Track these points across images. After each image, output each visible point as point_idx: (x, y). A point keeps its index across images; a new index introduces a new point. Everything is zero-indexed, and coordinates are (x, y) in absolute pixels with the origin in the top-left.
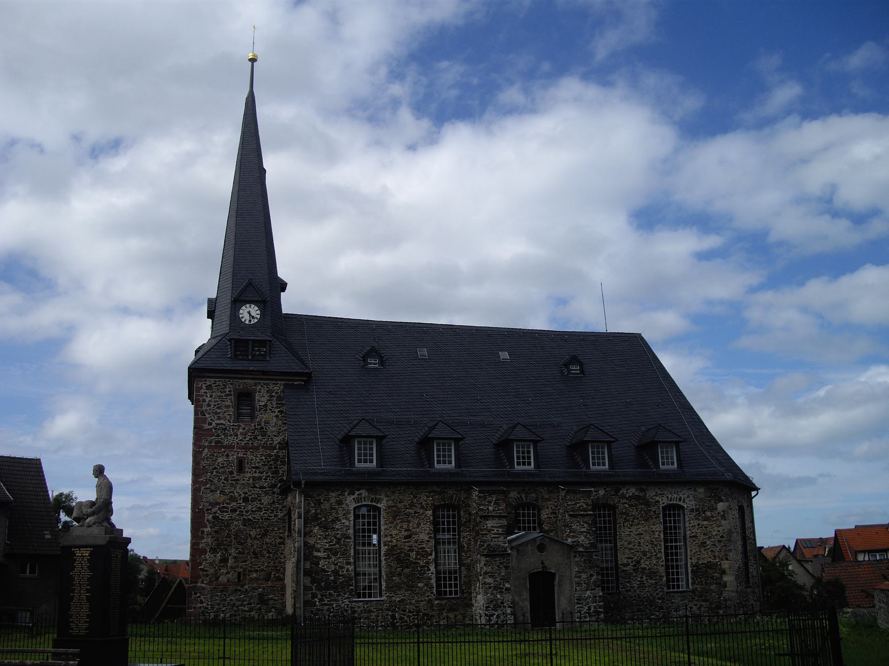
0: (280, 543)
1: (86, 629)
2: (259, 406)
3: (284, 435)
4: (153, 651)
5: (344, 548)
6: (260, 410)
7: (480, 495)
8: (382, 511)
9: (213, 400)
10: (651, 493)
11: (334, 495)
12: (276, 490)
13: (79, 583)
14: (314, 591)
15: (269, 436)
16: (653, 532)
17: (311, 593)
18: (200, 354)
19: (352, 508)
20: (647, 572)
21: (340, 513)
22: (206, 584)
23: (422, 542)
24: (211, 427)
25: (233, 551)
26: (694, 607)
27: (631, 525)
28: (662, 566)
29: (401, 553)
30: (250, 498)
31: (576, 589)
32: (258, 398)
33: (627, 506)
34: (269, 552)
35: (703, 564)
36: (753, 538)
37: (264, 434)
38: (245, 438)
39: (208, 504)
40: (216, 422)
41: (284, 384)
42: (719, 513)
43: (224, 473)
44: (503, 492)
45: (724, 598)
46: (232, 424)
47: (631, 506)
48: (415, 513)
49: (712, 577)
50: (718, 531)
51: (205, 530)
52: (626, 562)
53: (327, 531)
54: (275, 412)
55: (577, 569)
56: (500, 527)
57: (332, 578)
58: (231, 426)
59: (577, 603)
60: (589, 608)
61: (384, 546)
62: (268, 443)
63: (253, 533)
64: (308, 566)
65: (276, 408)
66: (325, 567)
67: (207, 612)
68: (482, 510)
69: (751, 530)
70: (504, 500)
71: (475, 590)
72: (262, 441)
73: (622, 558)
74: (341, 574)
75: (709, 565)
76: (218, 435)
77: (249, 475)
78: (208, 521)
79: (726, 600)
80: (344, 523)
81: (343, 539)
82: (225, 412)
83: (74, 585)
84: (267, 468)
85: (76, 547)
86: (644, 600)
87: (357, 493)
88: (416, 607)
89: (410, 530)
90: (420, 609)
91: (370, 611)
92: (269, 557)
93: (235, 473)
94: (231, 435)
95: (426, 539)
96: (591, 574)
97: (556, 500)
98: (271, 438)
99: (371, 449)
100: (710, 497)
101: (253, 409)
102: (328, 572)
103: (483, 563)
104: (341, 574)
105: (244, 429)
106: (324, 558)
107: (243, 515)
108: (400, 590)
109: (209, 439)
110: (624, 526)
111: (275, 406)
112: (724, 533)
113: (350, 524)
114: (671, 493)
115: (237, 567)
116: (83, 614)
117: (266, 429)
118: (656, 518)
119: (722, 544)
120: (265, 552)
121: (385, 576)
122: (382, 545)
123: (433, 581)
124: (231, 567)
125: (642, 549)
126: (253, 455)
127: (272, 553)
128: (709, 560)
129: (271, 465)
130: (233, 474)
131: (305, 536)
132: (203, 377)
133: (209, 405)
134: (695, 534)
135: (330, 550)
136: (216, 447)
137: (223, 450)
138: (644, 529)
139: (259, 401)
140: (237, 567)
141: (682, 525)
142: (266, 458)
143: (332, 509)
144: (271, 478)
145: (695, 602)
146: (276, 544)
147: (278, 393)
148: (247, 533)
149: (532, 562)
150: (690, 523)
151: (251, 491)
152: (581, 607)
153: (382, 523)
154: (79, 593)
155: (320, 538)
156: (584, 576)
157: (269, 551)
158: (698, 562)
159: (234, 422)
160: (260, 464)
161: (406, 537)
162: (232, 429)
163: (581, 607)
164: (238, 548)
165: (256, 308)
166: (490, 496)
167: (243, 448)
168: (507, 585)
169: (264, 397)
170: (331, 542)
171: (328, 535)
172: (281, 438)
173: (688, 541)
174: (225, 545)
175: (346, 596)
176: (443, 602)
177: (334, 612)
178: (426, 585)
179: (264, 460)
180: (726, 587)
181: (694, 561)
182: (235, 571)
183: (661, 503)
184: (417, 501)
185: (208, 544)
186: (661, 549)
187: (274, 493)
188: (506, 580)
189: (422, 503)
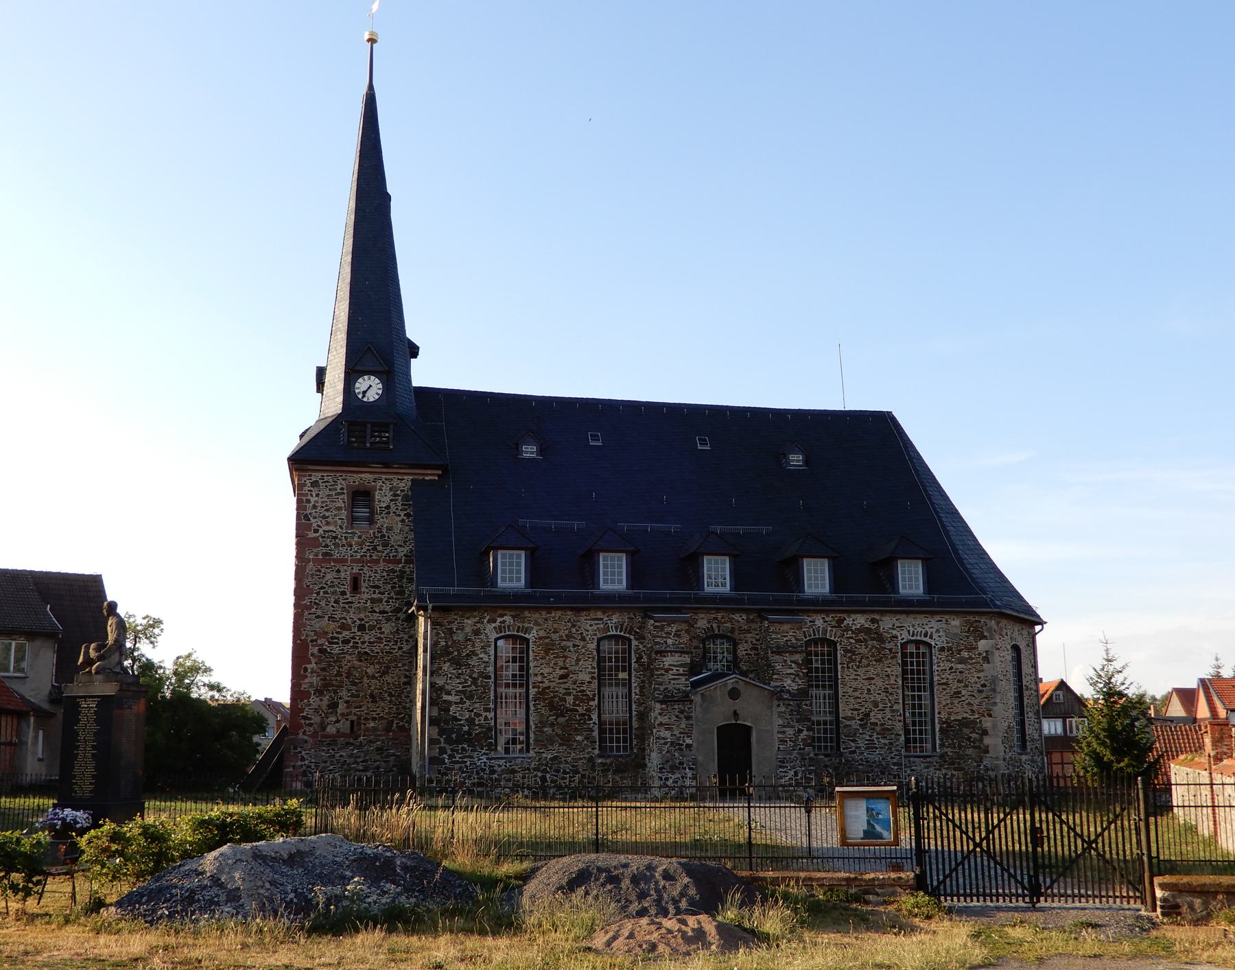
0: (405, 683)
1: (91, 792)
4: (1213, 806)
6: (381, 513)
7: (656, 624)
8: (531, 643)
9: (320, 500)
10: (887, 623)
11: (469, 622)
14: (442, 745)
15: (393, 546)
18: (306, 439)
19: (493, 640)
20: (878, 728)
22: (309, 736)
23: (582, 683)
24: (318, 534)
27: (858, 667)
28: (900, 721)
29: (555, 697)
30: (367, 625)
31: (779, 748)
33: (853, 641)
34: (390, 695)
35: (955, 720)
36: (1034, 688)
37: (385, 545)
38: (362, 549)
39: (313, 633)
40: (324, 528)
42: (980, 654)
43: (334, 593)
44: (685, 621)
45: (985, 766)
48: (574, 646)
50: (979, 678)
51: (309, 666)
54: (400, 515)
55: (781, 722)
56: (681, 666)
57: (466, 728)
59: (780, 767)
60: (796, 774)
61: (533, 688)
62: (391, 555)
64: (435, 713)
67: (310, 772)
68: (658, 643)
69: (1033, 678)
70: (687, 631)
71: (649, 745)
73: (844, 710)
74: (477, 723)
75: (964, 723)
76: (327, 546)
77: (365, 596)
78: (313, 655)
79: (987, 769)
81: (481, 679)
82: (335, 515)
83: (79, 741)
85: (81, 697)
86: (874, 765)
87: (499, 620)
88: (573, 766)
89: (567, 668)
90: (577, 770)
91: (513, 772)
92: (391, 702)
94: (343, 546)
95: (588, 680)
96: (799, 729)
98: (396, 549)
99: (519, 564)
100: (967, 632)
101: (372, 513)
102: (461, 720)
103: (657, 711)
104: (477, 723)
105: (360, 537)
106: (456, 703)
107: (357, 648)
108: (552, 745)
109: (315, 550)
111: (400, 508)
112: (986, 680)
113: (490, 659)
114: (913, 626)
115: (348, 714)
117: (388, 537)
118: (892, 658)
119: (984, 695)
120: (386, 695)
121: (533, 727)
122: (531, 687)
123: (596, 734)
124: (342, 715)
125: (873, 699)
128: (965, 715)
129: (396, 583)
131: (431, 675)
132: (307, 470)
133: (315, 507)
134: (945, 681)
136: (323, 561)
137: (332, 564)
138: (875, 673)
139: (380, 501)
140: (348, 714)
141: (927, 668)
143: (470, 640)
146: (399, 684)
147: (404, 491)
148: (362, 671)
149: (721, 713)
153: (531, 658)
156: (790, 731)
157: (390, 693)
158: (949, 718)
159: (347, 528)
161: (562, 677)
165: (377, 381)
166: (669, 625)
167: (358, 561)
168: (688, 741)
171: (462, 674)
173: (935, 689)
174: (333, 686)
175: (483, 751)
176: (608, 761)
178: (587, 738)
180: (988, 752)
181: (944, 716)
182: (347, 720)
183: (900, 638)
184: (576, 630)
185: (311, 685)
186: (898, 699)
188: (686, 733)
189: (582, 633)
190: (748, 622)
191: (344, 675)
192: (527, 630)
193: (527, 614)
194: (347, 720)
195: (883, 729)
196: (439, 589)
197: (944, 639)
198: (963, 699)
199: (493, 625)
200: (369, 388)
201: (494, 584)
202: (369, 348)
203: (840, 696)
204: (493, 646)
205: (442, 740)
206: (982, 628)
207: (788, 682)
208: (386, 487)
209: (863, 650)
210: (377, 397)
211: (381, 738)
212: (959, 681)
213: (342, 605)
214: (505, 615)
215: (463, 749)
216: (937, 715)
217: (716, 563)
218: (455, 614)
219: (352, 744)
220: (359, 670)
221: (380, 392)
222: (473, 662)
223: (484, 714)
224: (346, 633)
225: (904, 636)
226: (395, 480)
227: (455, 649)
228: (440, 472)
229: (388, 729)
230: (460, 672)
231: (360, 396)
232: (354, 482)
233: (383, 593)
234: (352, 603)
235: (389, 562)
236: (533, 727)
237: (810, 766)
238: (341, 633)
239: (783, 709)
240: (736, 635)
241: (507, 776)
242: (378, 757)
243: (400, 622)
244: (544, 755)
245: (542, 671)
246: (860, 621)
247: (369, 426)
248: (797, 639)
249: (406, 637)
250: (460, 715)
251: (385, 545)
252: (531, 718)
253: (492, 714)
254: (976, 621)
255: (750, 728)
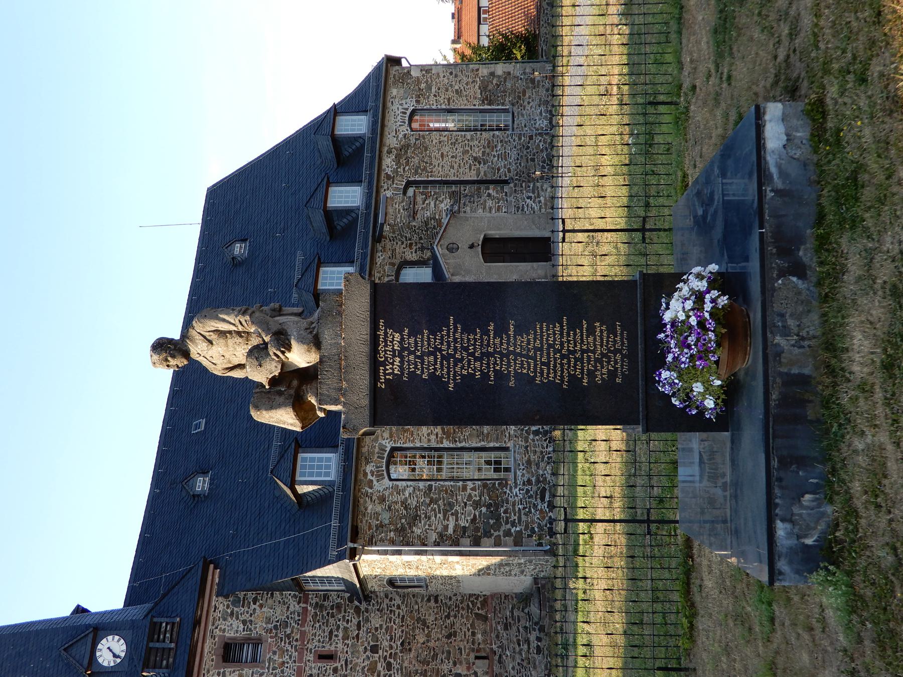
0: (436, 601)
1: (612, 331)
2: (244, 631)
3: (288, 595)
5: (443, 494)
6: (250, 630)
8: (396, 445)
10: (391, 141)
11: (370, 507)
12: (363, 606)
13: (479, 359)
14: (501, 533)
16: (440, 142)
17: (504, 537)
19: (391, 483)
20: (487, 150)
21: (396, 499)
25: (446, 667)
26: (531, 104)
28: (481, 134)
30: (372, 643)
32: (232, 633)
33: (407, 168)
34: (448, 617)
35: (481, 94)
38: (287, 650)
41: (217, 596)
42: (423, 75)
46: (267, 670)
47: (407, 164)
49: (498, 86)
50: (444, 77)
52: (475, 172)
53: (420, 516)
54: (255, 609)
55: (481, 211)
57: (484, 509)
58: (269, 671)
59: (523, 210)
61: (442, 443)
62: (297, 618)
63: (421, 639)
65: (249, 608)
66: (469, 518)
72: (293, 627)
74: (478, 498)
75: (484, 88)
77: (340, 646)
80: (410, 494)
83: (485, 376)
84: (331, 620)
86: (520, 154)
87: (370, 477)
91: (529, 462)
92: (455, 617)
93: (335, 665)
94: (282, 672)
96: (487, 196)
97: (395, 243)
98: (291, 614)
99: (313, 459)
100: (403, 84)
101: (248, 640)
102: (475, 515)
104: (478, 498)
105: (274, 653)
106: (457, 520)
107: (396, 654)
110: (431, 172)
111: (246, 609)
113: (411, 486)
114: (396, 122)
116: (569, 341)
117: (277, 621)
120: (448, 621)
121: (483, 443)
122: (442, 446)
124: (468, 669)
126: (313, 639)
127: (449, 613)
128: (477, 87)
129: (328, 614)
130: (337, 667)
135: (445, 512)
142: (319, 622)
143: (389, 507)
144: (347, 614)
145: (526, 103)
150: (433, 105)
151: (363, 642)
152: (527, 206)
153: (412, 445)
154: (507, 356)
155: (430, 526)
156: (489, 203)
157: (446, 617)
158: (479, 99)
159: (263, 668)
160: (326, 629)
162: (273, 670)
163: (527, 206)
164: (442, 660)
165: (104, 641)
169: (231, 624)
170: (435, 510)
172: (291, 601)
175: (508, 491)
177: (530, 506)
179: (321, 623)
180: (509, 73)
181: (477, 102)
182: (474, 664)
183: (406, 132)
187: (367, 610)
190: (385, 251)
191: (425, 667)
192: (383, 449)
193: (365, 450)
194: (474, 664)
195: (488, 147)
196: (333, 540)
197: (408, 101)
198: (462, 88)
199: (375, 482)
200: (111, 651)
201: (331, 484)
202: (65, 650)
203: (458, 179)
204: (397, 483)
205: (496, 534)
206: (400, 74)
207: (443, 206)
208: (222, 625)
209: (416, 160)
210: (122, 641)
211: (494, 625)
212: (447, 90)
213: (348, 671)
214: (364, 471)
215: (506, 512)
216: (477, 107)
217: (326, 278)
218: (361, 522)
219: (500, 656)
220: (420, 651)
221: (117, 638)
222: (413, 502)
223: (469, 491)
224: (379, 667)
225: (405, 129)
226: (215, 615)
227: (398, 521)
228: (212, 566)
229: (485, 619)
230: (423, 516)
231: (118, 660)
232: (212, 660)
233: (338, 627)
234: (346, 660)
235: (304, 621)
236: (483, 443)
237: (522, 187)
238: (380, 672)
239: (468, 209)
240: (397, 261)
241: (534, 467)
242: (514, 628)
243: (370, 608)
244: (512, 432)
245: (425, 435)
246: (388, 163)
247: (151, 645)
248: (402, 202)
249: (387, 601)
250: (469, 515)
251: (286, 624)
252: (474, 445)
253: (469, 483)
254: (394, 77)
255: (485, 235)
